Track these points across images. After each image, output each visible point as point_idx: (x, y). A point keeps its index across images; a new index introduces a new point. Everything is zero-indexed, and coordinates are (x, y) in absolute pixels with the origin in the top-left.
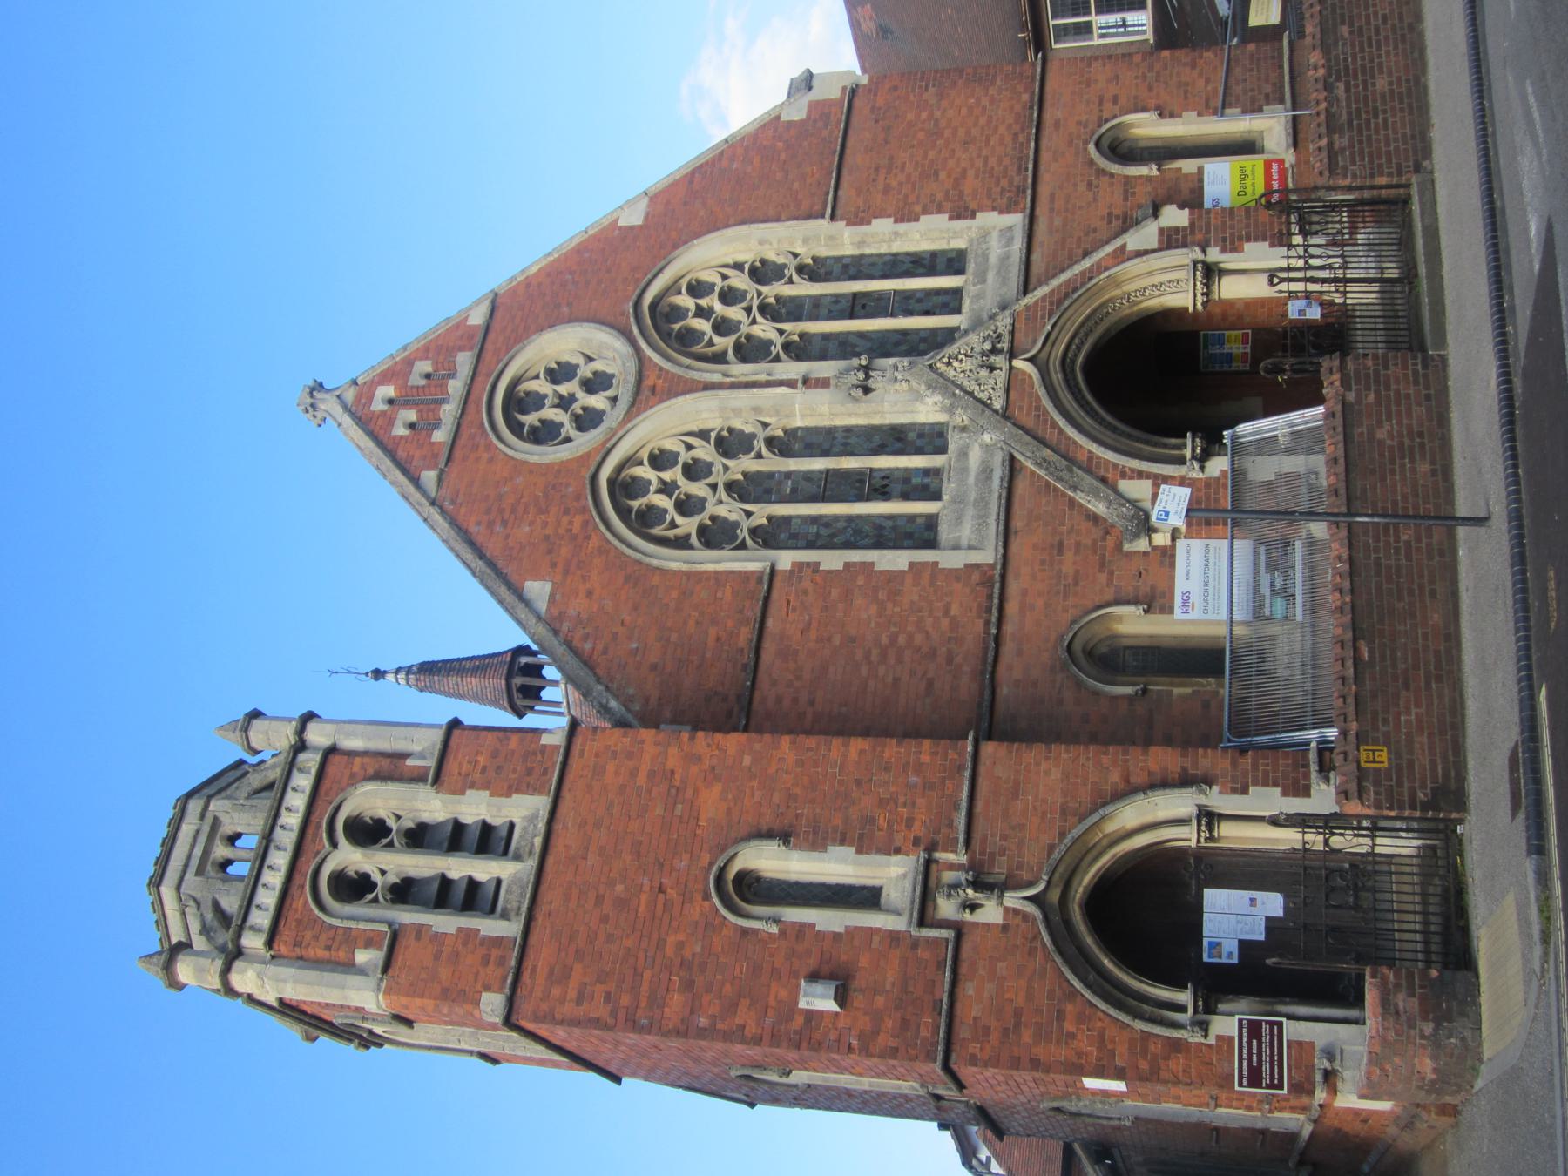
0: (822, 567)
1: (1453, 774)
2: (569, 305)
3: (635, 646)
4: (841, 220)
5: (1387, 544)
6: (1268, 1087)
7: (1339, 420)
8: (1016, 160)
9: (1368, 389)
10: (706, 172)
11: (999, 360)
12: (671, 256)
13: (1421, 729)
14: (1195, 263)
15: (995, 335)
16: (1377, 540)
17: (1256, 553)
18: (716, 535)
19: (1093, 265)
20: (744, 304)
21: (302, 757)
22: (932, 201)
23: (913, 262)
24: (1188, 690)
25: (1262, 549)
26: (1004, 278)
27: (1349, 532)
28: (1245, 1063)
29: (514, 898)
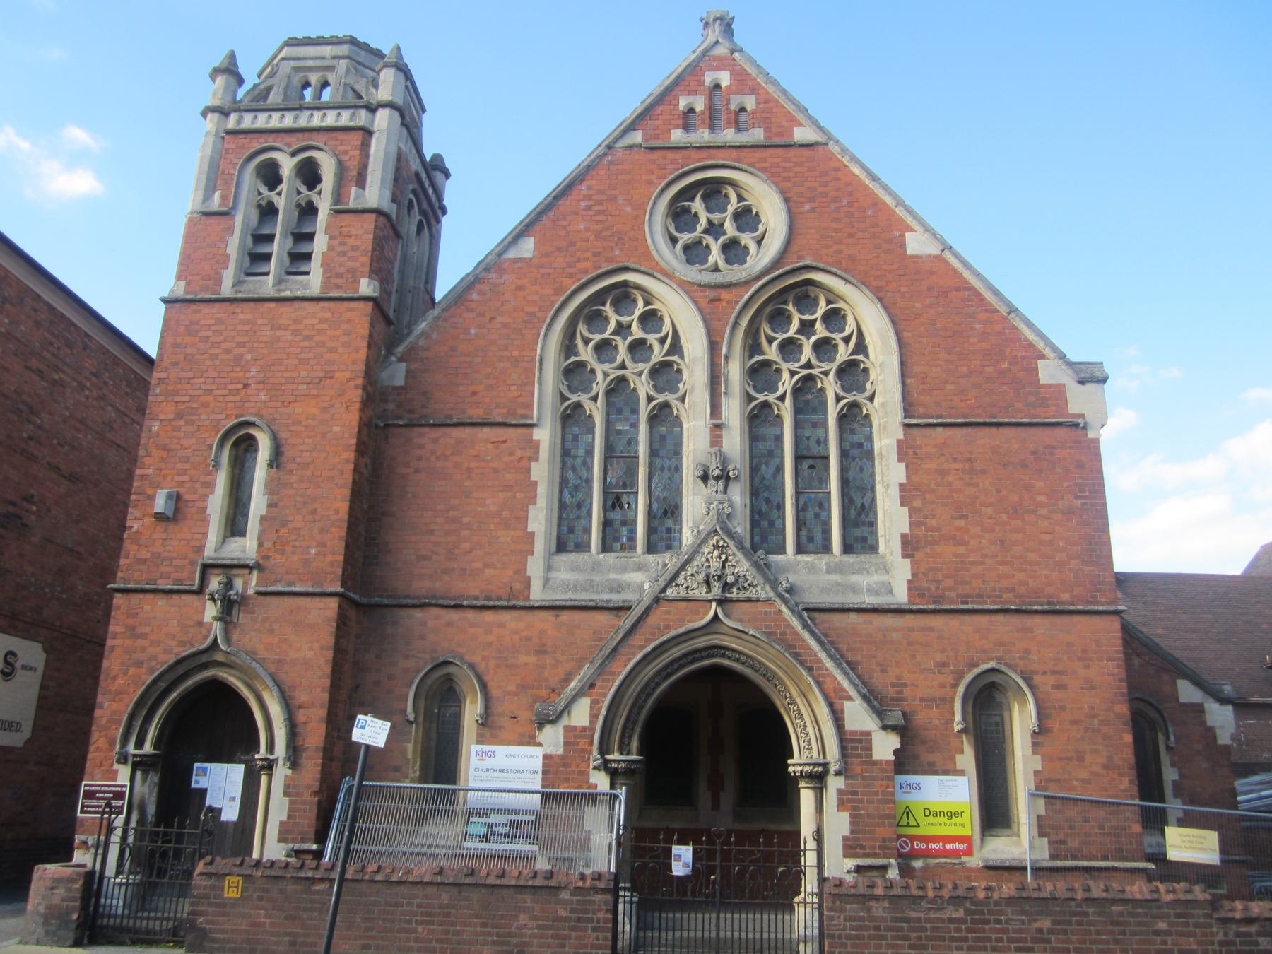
0: (533, 464)
1: (216, 945)
2: (813, 210)
3: (473, 331)
4: (905, 435)
5: (416, 914)
6: (83, 804)
7: (538, 882)
8: (977, 591)
9: (572, 911)
10: (972, 301)
11: (716, 590)
12: (863, 288)
13: (254, 925)
14: (825, 765)
15: (746, 585)
16: (419, 906)
17: (527, 812)
18: (574, 373)
19: (827, 669)
20: (814, 361)
21: (363, 112)
22: (926, 517)
23: (863, 506)
24: (410, 756)
25: (532, 818)
26: (830, 590)
27: (427, 883)
28: (98, 788)
29: (251, 287)
